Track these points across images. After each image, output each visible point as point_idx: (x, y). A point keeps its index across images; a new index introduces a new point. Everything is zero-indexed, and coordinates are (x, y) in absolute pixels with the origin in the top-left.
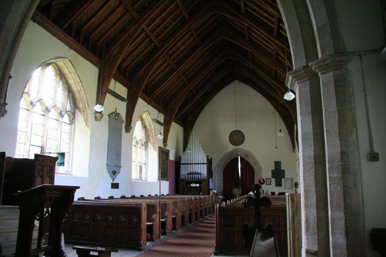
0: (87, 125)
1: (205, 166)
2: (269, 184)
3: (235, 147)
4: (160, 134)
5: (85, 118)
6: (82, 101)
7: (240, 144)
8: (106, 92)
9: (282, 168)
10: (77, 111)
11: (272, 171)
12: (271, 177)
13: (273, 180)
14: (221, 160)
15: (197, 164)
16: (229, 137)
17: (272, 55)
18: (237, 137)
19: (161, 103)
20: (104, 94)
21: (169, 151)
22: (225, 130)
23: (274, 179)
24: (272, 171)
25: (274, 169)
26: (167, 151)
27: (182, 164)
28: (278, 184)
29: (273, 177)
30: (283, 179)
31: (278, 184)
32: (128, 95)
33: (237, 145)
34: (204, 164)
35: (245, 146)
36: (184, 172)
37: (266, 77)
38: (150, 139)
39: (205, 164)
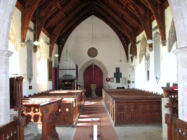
0: (16, 50)
1: (75, 70)
2: (113, 81)
3: (92, 58)
4: (57, 54)
5: (15, 46)
6: (13, 34)
7: (95, 57)
8: (27, 29)
9: (120, 72)
10: (9, 41)
11: (114, 73)
12: (113, 77)
13: (115, 79)
14: (83, 67)
15: (72, 69)
16: (88, 52)
17: (123, 5)
18: (93, 52)
19: (50, 33)
20: (26, 30)
21: (52, 61)
22: (85, 47)
23: (115, 78)
24: (114, 73)
25: (115, 72)
26: (51, 62)
27: (60, 70)
28: (118, 81)
29: (114, 77)
30: (121, 78)
31: (118, 81)
32: (35, 27)
33: (93, 57)
34: (74, 69)
35: (97, 58)
36: (61, 75)
37: (115, 17)
38: (42, 54)
39: (75, 69)
